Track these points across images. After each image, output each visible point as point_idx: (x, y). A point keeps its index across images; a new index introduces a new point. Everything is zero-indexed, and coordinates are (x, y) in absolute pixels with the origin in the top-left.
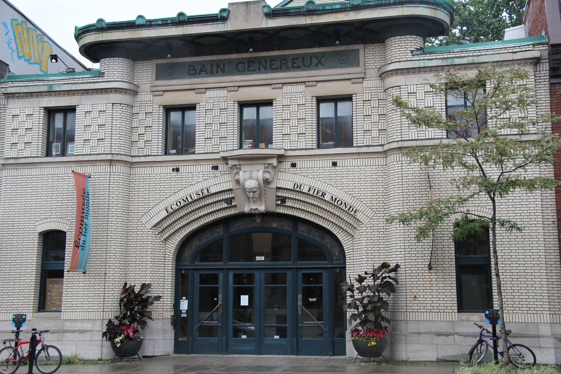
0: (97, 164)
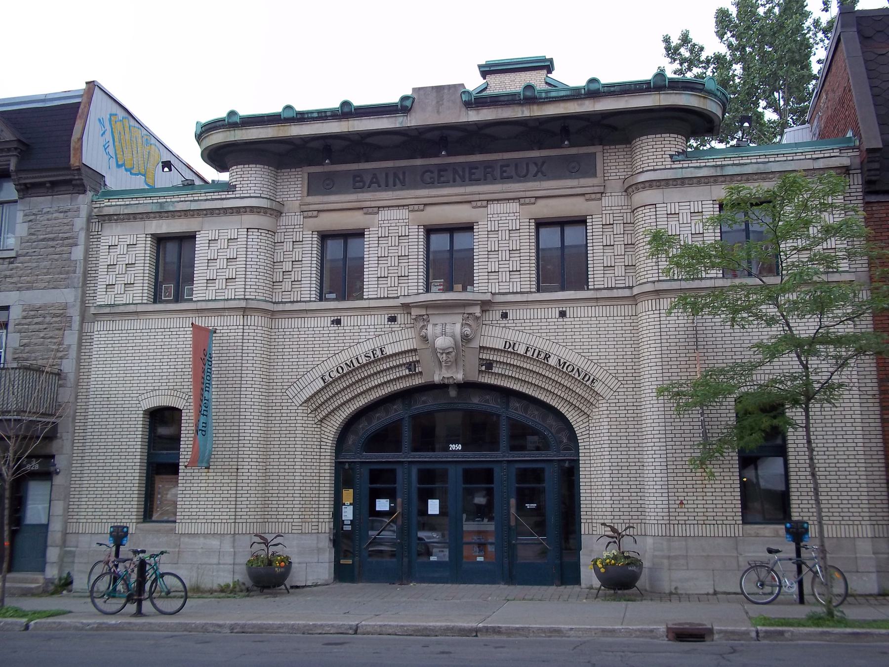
0: (225, 314)
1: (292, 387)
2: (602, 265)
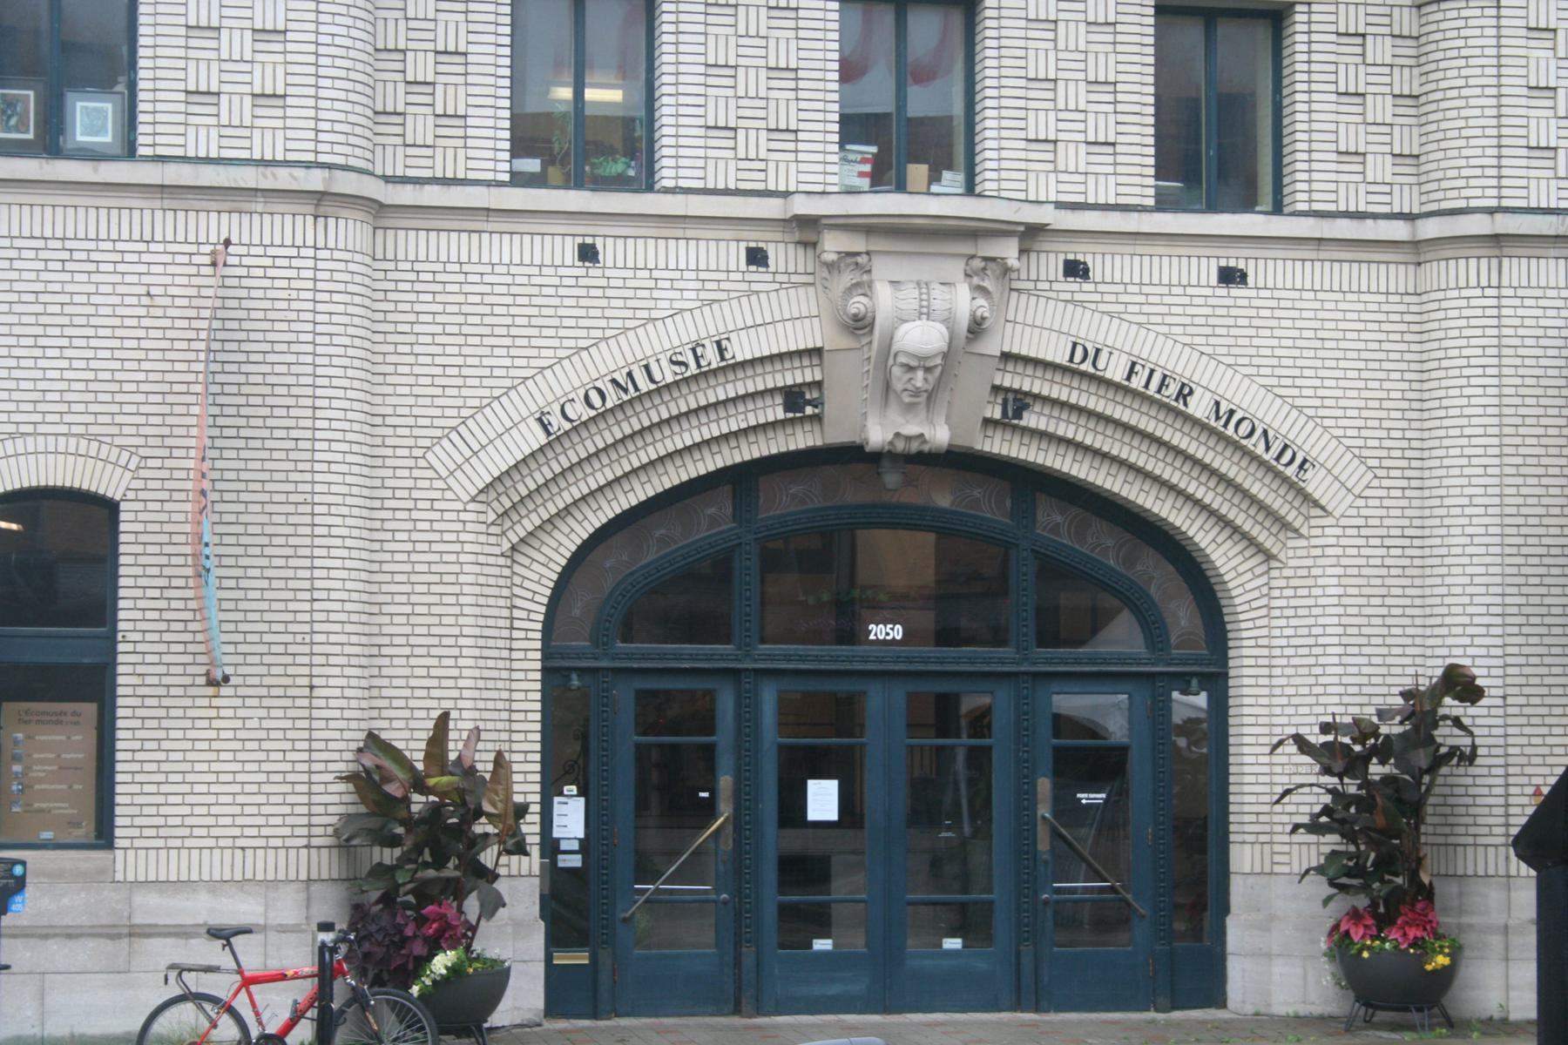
0: (253, 207)
2: (1333, 147)
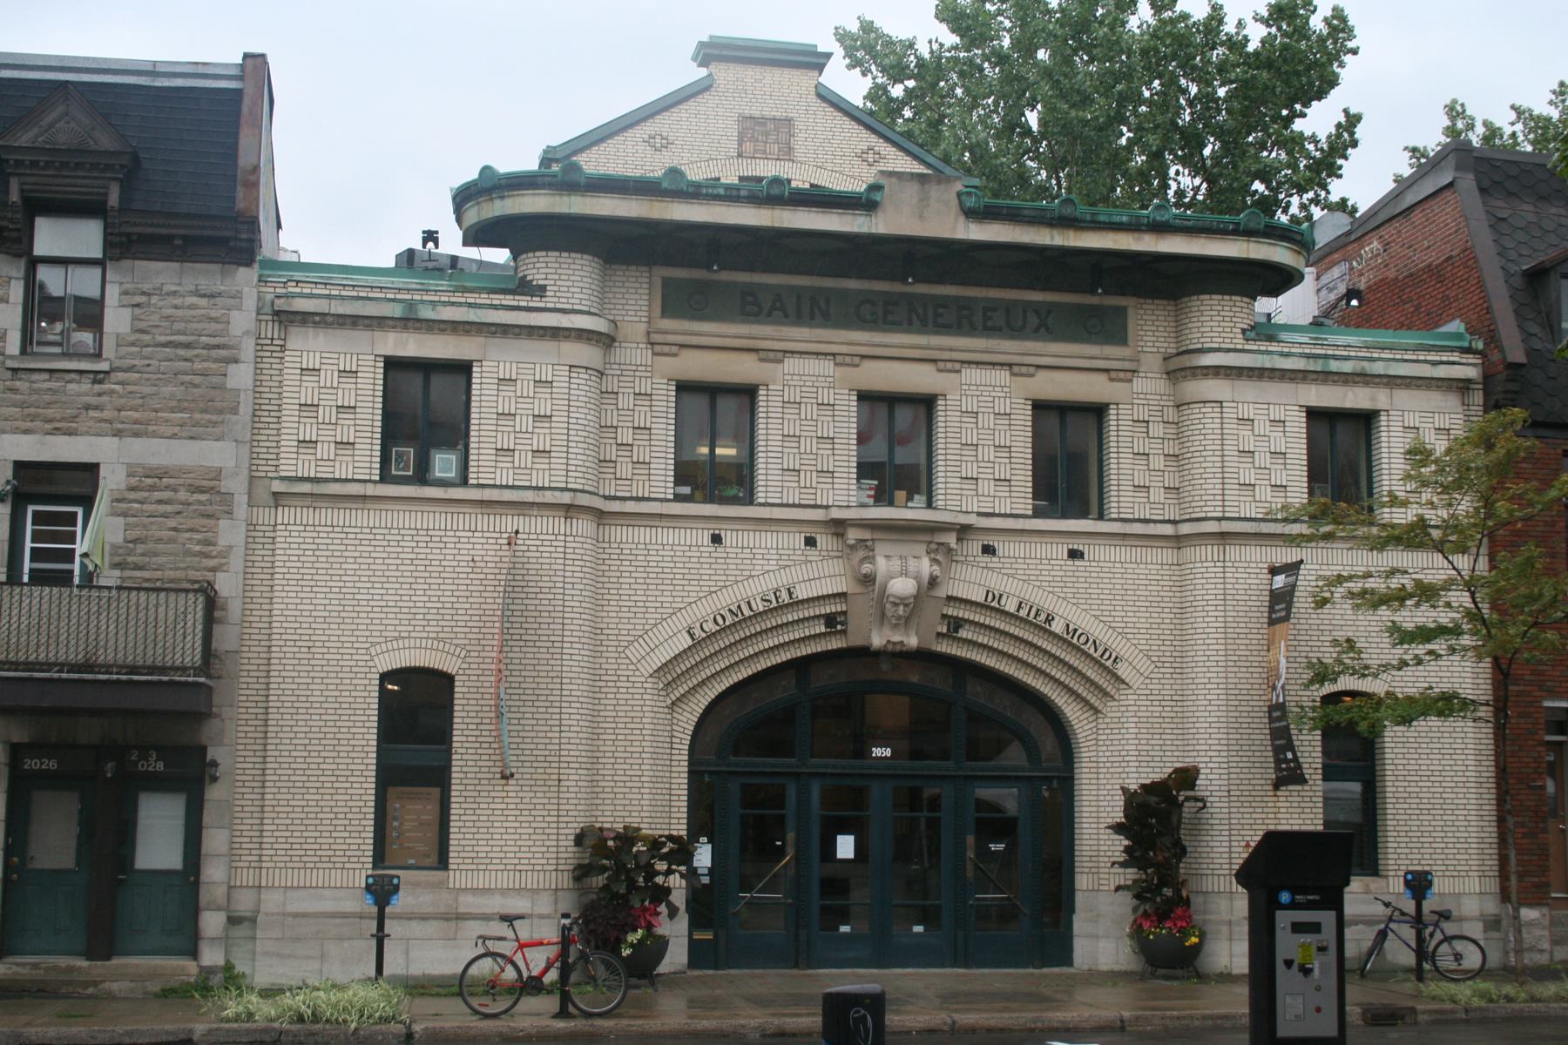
1: (636, 644)
